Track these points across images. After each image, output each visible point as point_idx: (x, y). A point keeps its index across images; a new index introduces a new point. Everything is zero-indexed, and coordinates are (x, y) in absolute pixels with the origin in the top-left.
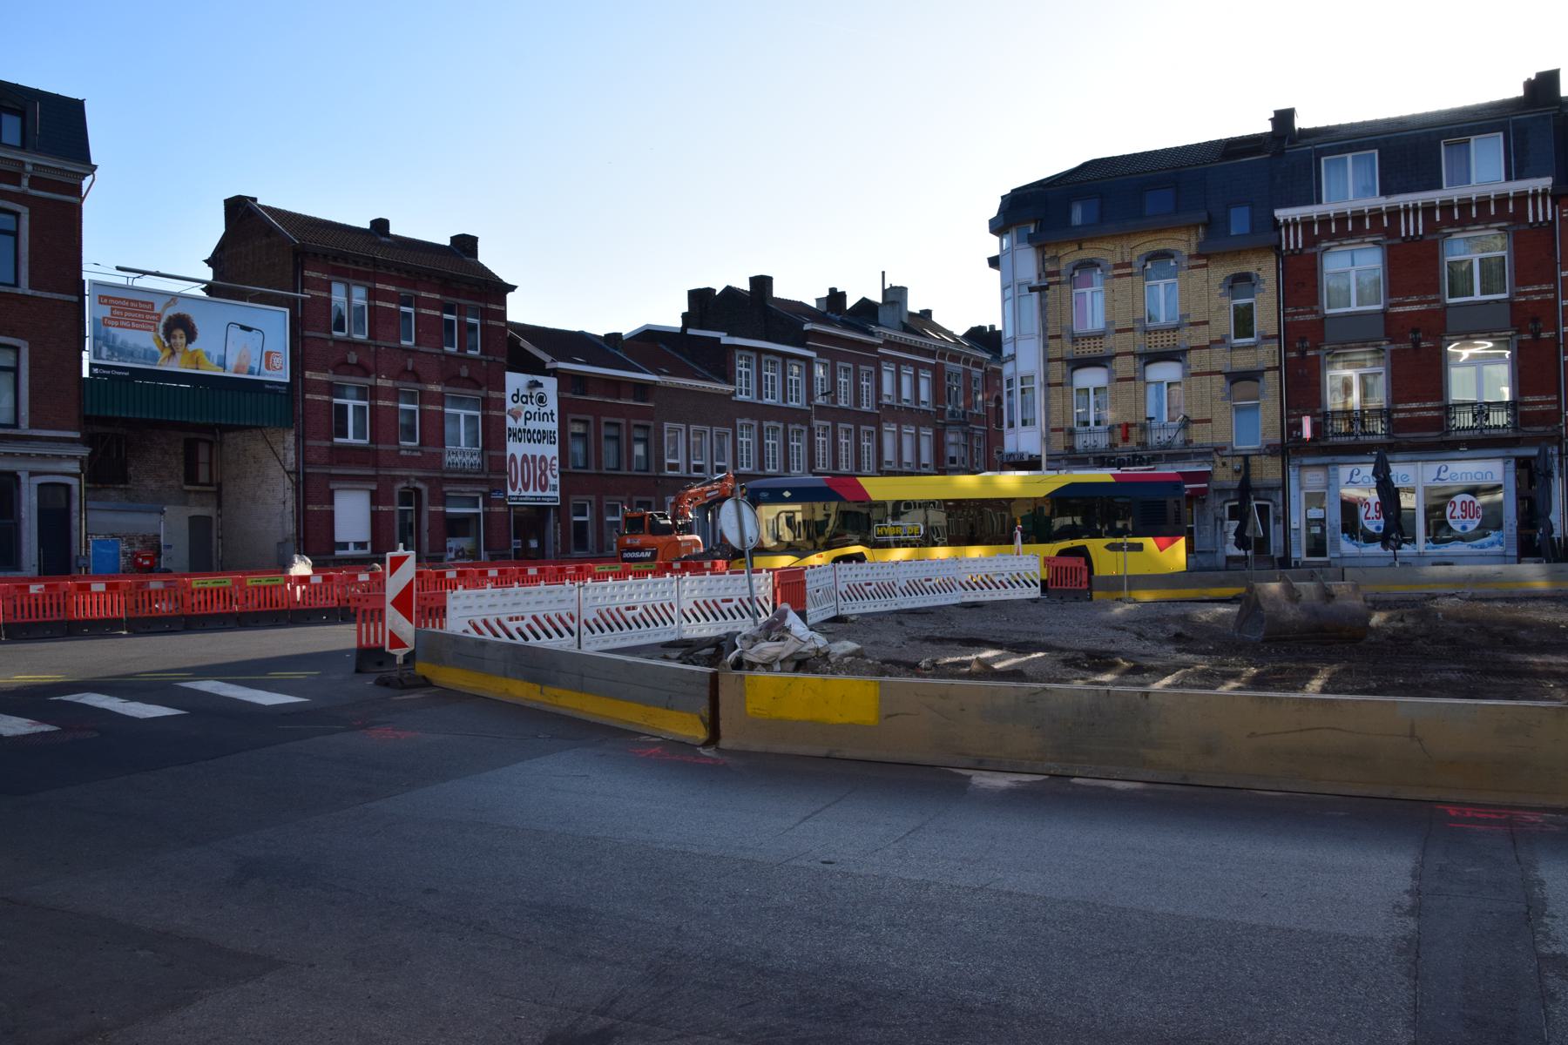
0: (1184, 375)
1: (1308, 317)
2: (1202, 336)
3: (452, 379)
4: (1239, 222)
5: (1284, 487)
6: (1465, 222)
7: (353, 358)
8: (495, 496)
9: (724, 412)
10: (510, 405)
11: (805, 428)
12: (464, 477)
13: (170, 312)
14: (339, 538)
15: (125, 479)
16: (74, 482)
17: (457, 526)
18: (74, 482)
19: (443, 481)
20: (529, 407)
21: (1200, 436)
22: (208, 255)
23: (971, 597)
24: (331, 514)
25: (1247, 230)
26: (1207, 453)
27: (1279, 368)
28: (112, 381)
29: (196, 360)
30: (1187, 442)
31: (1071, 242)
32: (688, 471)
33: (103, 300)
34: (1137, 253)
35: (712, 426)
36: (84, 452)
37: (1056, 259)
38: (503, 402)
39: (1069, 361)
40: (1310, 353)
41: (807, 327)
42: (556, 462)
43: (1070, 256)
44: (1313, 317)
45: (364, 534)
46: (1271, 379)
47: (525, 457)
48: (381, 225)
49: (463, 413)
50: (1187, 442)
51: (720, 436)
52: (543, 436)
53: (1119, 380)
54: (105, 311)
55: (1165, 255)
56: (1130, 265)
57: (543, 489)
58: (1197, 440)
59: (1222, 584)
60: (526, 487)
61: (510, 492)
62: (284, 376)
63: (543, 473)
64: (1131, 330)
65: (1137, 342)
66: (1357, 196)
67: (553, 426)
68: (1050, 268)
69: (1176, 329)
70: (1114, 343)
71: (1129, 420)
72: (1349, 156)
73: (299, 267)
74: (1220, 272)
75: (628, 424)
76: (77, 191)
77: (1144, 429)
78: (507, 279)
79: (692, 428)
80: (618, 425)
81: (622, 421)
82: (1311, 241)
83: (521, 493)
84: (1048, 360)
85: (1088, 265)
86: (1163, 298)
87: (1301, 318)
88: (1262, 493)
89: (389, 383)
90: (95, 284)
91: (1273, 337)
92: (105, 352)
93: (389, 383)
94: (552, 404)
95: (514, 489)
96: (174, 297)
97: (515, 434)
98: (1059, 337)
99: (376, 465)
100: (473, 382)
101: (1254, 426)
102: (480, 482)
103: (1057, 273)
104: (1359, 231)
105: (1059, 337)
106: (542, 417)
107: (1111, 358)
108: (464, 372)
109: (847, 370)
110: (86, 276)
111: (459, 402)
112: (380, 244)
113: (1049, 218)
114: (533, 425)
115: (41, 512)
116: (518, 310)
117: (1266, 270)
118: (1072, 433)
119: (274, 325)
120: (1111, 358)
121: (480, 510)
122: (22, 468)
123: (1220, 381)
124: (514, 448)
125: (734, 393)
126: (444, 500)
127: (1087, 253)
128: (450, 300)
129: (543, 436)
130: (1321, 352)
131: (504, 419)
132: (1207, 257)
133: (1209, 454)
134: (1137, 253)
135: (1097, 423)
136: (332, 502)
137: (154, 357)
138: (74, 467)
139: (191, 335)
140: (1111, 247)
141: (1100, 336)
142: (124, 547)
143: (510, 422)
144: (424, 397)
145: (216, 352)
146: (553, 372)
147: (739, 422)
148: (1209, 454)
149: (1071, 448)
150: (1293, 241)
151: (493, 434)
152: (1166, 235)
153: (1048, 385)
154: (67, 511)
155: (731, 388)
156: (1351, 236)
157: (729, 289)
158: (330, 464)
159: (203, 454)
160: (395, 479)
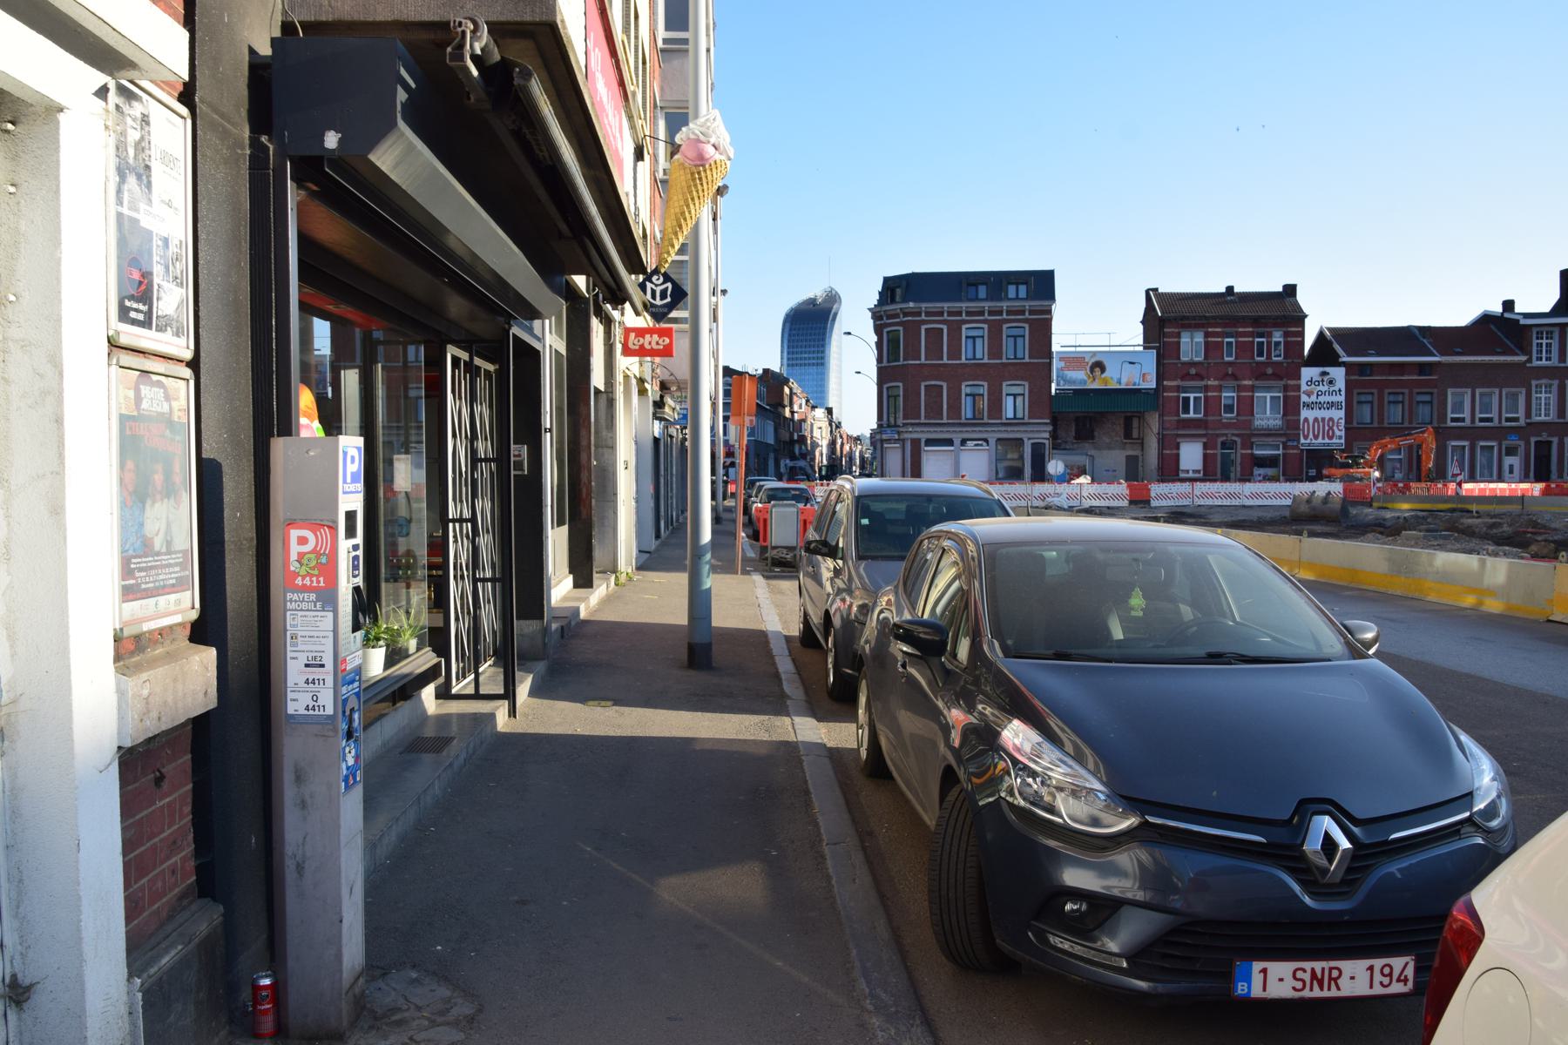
7: (1193, 371)
10: (1304, 387)
12: (1268, 433)
15: (1093, 438)
17: (1270, 462)
19: (1250, 436)
20: (1321, 388)
28: (1062, 394)
32: (1473, 421)
33: (1061, 359)
38: (1298, 388)
45: (1199, 465)
47: (1316, 420)
48: (1230, 289)
52: (1331, 405)
54: (1062, 364)
57: (1331, 438)
63: (1331, 428)
67: (1342, 398)
75: (1411, 393)
76: (1049, 312)
79: (1478, 391)
94: (1341, 384)
95: (1306, 437)
96: (1095, 353)
97: (1307, 405)
106: (1330, 394)
108: (1270, 371)
111: (1268, 389)
114: (1321, 399)
124: (1305, 413)
125: (1530, 360)
129: (1331, 405)
138: (1047, 435)
139: (1103, 369)
143: (1304, 398)
147: (1534, 383)
151: (1291, 406)
155: (1524, 358)
159: (1135, 423)
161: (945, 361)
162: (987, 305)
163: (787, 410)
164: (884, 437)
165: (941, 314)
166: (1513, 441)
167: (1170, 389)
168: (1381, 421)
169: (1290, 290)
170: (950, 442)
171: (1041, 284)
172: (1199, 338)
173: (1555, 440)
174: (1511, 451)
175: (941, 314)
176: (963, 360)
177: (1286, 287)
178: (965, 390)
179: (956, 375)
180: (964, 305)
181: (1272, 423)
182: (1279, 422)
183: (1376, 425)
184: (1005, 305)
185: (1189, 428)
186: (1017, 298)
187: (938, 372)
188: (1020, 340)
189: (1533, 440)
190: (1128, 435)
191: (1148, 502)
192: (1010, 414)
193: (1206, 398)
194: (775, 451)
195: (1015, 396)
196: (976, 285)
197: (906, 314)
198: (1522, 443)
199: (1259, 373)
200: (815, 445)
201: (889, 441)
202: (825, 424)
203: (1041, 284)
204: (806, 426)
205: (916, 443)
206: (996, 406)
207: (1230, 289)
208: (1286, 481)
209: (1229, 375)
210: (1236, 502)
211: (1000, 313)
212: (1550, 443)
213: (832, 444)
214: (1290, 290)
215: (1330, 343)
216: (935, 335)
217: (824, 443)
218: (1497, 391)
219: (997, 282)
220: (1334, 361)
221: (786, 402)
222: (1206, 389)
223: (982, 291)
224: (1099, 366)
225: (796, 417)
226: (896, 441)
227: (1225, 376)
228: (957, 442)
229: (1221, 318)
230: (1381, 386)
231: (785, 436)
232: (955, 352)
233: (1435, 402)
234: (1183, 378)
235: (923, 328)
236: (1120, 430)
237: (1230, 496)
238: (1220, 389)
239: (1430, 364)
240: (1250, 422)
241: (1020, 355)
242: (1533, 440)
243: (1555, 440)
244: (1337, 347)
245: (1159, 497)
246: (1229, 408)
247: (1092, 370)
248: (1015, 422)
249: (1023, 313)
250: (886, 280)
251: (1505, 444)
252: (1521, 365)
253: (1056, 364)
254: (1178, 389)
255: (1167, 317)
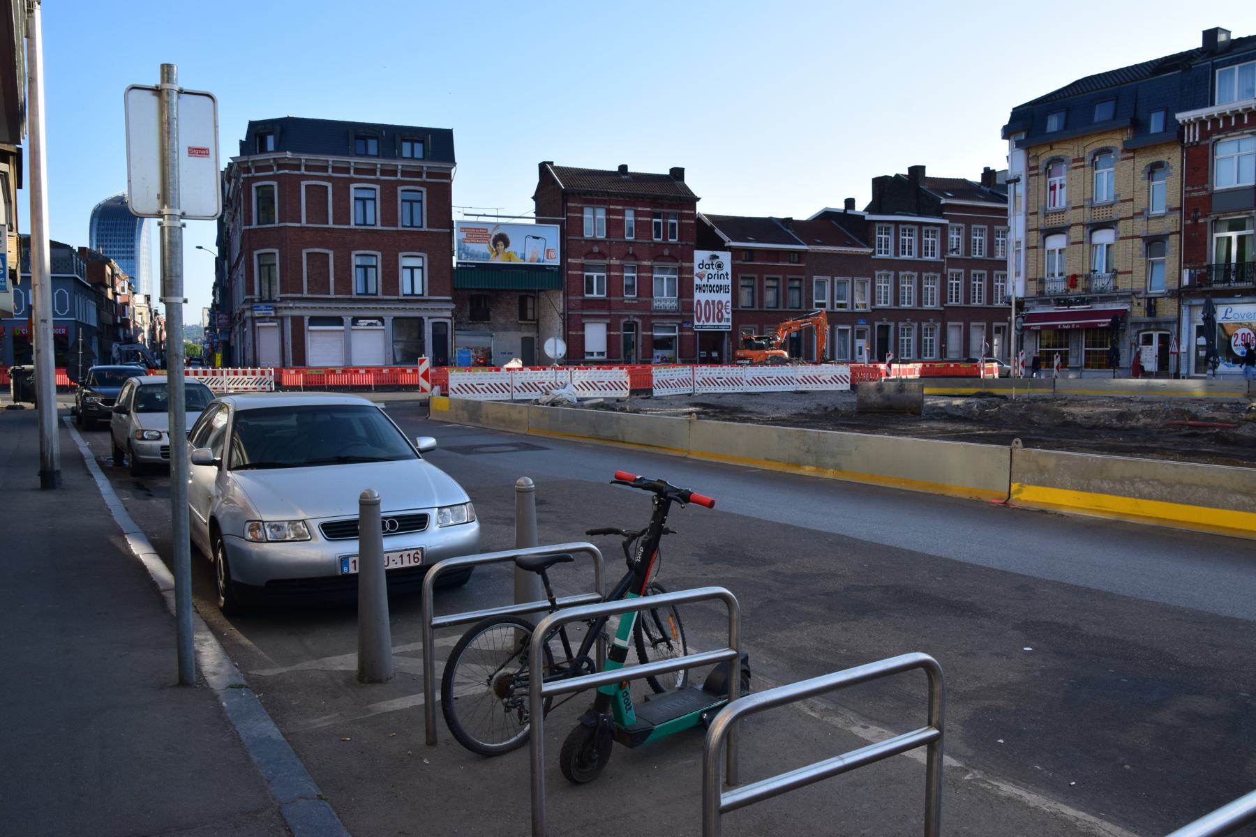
0: (1116, 239)
1: (1201, 193)
2: (1127, 210)
3: (658, 257)
4: (1156, 124)
5: (1178, 321)
6: (1228, 129)
7: (596, 249)
8: (685, 325)
9: (865, 268)
10: (697, 270)
11: (939, 275)
12: (666, 315)
13: (496, 232)
14: (587, 350)
15: (488, 318)
16: (449, 321)
17: (665, 344)
18: (449, 321)
19: (651, 317)
20: (711, 271)
21: (1124, 284)
22: (533, 194)
23: (803, 387)
24: (583, 336)
25: (1161, 129)
26: (1131, 295)
27: (1180, 233)
28: (464, 269)
29: (509, 257)
30: (1116, 288)
31: (1045, 145)
32: (832, 307)
33: (463, 230)
34: (1088, 150)
35: (853, 277)
36: (453, 306)
37: (1037, 157)
38: (692, 269)
39: (1042, 231)
40: (1201, 221)
41: (943, 201)
42: (730, 304)
43: (1046, 154)
44: (1204, 193)
45: (603, 348)
46: (1174, 241)
47: (707, 302)
48: (623, 168)
49: (665, 277)
50: (1116, 288)
51: (863, 284)
52: (720, 288)
53: (1073, 243)
54: (464, 235)
55: (1106, 151)
56: (1083, 159)
57: (720, 320)
58: (1121, 287)
59: (968, 386)
60: (708, 320)
61: (696, 323)
62: (556, 261)
63: (720, 311)
64: (1082, 207)
65: (1087, 216)
66: (1241, 98)
67: (728, 282)
68: (1032, 164)
69: (1111, 205)
70: (1072, 217)
71: (1077, 272)
72: (1236, 67)
73: (565, 201)
74: (1143, 162)
75: (784, 280)
76: (449, 176)
77: (1088, 278)
78: (697, 194)
79: (836, 279)
80: (777, 279)
81: (781, 277)
82: (1205, 135)
83: (702, 323)
84: (1028, 230)
85: (1057, 161)
86: (1107, 182)
87: (1196, 194)
88: (1163, 326)
89: (618, 262)
90: (459, 222)
91: (1176, 209)
92: (464, 256)
93: (618, 262)
94: (727, 268)
95: (699, 320)
96: (498, 225)
97: (700, 288)
98: (1036, 213)
99: (610, 309)
100: (673, 258)
101: (1169, 272)
102: (676, 317)
103: (1037, 168)
104: (1240, 126)
105: (1036, 213)
106: (719, 277)
107: (1068, 227)
108: (666, 252)
109: (981, 230)
110: (454, 218)
111: (663, 270)
112: (623, 181)
113: (1027, 125)
114: (712, 282)
115: (434, 336)
116: (702, 209)
117: (1174, 158)
118: (1042, 282)
119: (552, 234)
120: (1068, 227)
121: (676, 334)
122: (425, 315)
123: (1139, 243)
124: (698, 296)
125: (874, 253)
126: (651, 328)
127: (1056, 153)
128: (658, 210)
129: (720, 288)
130: (1209, 220)
131: (692, 279)
132: (1134, 151)
133: (1129, 297)
134: (1088, 150)
135: (1061, 274)
136: (583, 330)
137: (488, 257)
138: (449, 314)
139: (507, 244)
140: (1071, 147)
141: (1062, 212)
142: (472, 353)
143: (697, 281)
144: (640, 269)
145: (520, 252)
146: (730, 249)
147: (877, 273)
148: (1129, 297)
149: (1041, 293)
150: (1192, 136)
151: (685, 289)
152: (1107, 136)
153: (1028, 248)
154: (446, 336)
155: (870, 250)
156: (1233, 129)
157: (897, 175)
158: (582, 309)
159: (530, 304)
160: (621, 316)
161: (331, 225)
162: (379, 162)
163: (110, 291)
164: (256, 314)
165: (325, 169)
166: (862, 325)
167: (574, 267)
168: (761, 305)
169: (678, 173)
170: (338, 321)
171: (439, 144)
172: (601, 214)
173: (892, 325)
174: (861, 334)
175: (325, 169)
176: (352, 225)
177: (674, 170)
178: (355, 261)
179: (346, 242)
180: (353, 160)
181: (668, 304)
182: (675, 304)
183: (757, 308)
184: (400, 164)
185: (592, 308)
186: (412, 158)
187: (324, 237)
188: (416, 206)
189: (877, 324)
190: (523, 316)
191: (650, 391)
192: (407, 290)
193: (608, 277)
194: (99, 334)
195: (412, 269)
196: (365, 139)
197: (280, 167)
198: (868, 327)
199: (657, 254)
200: (138, 331)
201: (262, 319)
202: (145, 311)
203: (439, 144)
204: (129, 310)
205: (298, 322)
206: (391, 279)
207: (623, 168)
208: (684, 363)
209: (630, 254)
210: (791, 388)
211: (394, 173)
212: (888, 327)
213: (152, 330)
214: (678, 173)
215: (712, 229)
216: (317, 194)
217: (146, 328)
218: (829, 279)
219: (390, 138)
220: (720, 246)
221: (108, 282)
222: (609, 268)
223: (373, 146)
224: (502, 239)
225: (119, 299)
226: (272, 319)
227: (626, 256)
228: (347, 320)
229: (622, 195)
230: (761, 270)
231: (110, 320)
232: (343, 216)
233: (804, 288)
234: (586, 257)
235: (304, 184)
236: (515, 310)
237: (731, 381)
238: (621, 268)
239: (799, 252)
240: (650, 303)
241: (417, 222)
242: (877, 324)
243: (892, 325)
244: (718, 231)
245: (666, 384)
246: (630, 288)
247: (495, 244)
248: (412, 299)
249: (419, 174)
250: (252, 125)
251: (856, 327)
252: (868, 256)
253: (457, 235)
254: (583, 267)
255: (560, 192)
